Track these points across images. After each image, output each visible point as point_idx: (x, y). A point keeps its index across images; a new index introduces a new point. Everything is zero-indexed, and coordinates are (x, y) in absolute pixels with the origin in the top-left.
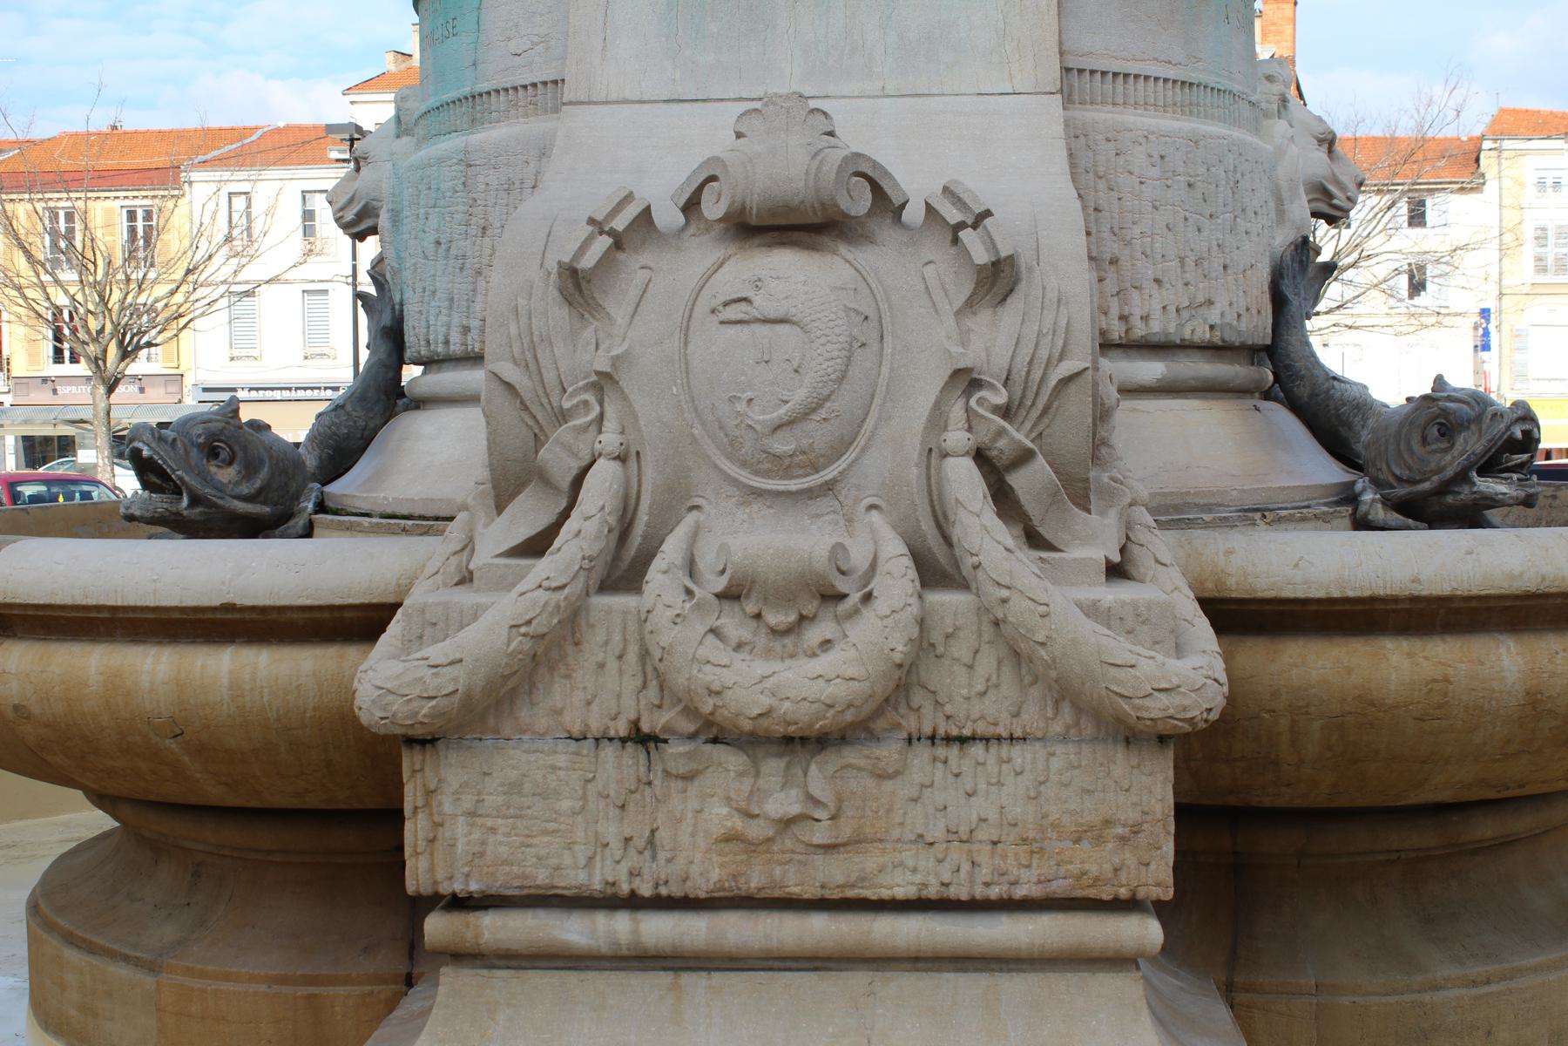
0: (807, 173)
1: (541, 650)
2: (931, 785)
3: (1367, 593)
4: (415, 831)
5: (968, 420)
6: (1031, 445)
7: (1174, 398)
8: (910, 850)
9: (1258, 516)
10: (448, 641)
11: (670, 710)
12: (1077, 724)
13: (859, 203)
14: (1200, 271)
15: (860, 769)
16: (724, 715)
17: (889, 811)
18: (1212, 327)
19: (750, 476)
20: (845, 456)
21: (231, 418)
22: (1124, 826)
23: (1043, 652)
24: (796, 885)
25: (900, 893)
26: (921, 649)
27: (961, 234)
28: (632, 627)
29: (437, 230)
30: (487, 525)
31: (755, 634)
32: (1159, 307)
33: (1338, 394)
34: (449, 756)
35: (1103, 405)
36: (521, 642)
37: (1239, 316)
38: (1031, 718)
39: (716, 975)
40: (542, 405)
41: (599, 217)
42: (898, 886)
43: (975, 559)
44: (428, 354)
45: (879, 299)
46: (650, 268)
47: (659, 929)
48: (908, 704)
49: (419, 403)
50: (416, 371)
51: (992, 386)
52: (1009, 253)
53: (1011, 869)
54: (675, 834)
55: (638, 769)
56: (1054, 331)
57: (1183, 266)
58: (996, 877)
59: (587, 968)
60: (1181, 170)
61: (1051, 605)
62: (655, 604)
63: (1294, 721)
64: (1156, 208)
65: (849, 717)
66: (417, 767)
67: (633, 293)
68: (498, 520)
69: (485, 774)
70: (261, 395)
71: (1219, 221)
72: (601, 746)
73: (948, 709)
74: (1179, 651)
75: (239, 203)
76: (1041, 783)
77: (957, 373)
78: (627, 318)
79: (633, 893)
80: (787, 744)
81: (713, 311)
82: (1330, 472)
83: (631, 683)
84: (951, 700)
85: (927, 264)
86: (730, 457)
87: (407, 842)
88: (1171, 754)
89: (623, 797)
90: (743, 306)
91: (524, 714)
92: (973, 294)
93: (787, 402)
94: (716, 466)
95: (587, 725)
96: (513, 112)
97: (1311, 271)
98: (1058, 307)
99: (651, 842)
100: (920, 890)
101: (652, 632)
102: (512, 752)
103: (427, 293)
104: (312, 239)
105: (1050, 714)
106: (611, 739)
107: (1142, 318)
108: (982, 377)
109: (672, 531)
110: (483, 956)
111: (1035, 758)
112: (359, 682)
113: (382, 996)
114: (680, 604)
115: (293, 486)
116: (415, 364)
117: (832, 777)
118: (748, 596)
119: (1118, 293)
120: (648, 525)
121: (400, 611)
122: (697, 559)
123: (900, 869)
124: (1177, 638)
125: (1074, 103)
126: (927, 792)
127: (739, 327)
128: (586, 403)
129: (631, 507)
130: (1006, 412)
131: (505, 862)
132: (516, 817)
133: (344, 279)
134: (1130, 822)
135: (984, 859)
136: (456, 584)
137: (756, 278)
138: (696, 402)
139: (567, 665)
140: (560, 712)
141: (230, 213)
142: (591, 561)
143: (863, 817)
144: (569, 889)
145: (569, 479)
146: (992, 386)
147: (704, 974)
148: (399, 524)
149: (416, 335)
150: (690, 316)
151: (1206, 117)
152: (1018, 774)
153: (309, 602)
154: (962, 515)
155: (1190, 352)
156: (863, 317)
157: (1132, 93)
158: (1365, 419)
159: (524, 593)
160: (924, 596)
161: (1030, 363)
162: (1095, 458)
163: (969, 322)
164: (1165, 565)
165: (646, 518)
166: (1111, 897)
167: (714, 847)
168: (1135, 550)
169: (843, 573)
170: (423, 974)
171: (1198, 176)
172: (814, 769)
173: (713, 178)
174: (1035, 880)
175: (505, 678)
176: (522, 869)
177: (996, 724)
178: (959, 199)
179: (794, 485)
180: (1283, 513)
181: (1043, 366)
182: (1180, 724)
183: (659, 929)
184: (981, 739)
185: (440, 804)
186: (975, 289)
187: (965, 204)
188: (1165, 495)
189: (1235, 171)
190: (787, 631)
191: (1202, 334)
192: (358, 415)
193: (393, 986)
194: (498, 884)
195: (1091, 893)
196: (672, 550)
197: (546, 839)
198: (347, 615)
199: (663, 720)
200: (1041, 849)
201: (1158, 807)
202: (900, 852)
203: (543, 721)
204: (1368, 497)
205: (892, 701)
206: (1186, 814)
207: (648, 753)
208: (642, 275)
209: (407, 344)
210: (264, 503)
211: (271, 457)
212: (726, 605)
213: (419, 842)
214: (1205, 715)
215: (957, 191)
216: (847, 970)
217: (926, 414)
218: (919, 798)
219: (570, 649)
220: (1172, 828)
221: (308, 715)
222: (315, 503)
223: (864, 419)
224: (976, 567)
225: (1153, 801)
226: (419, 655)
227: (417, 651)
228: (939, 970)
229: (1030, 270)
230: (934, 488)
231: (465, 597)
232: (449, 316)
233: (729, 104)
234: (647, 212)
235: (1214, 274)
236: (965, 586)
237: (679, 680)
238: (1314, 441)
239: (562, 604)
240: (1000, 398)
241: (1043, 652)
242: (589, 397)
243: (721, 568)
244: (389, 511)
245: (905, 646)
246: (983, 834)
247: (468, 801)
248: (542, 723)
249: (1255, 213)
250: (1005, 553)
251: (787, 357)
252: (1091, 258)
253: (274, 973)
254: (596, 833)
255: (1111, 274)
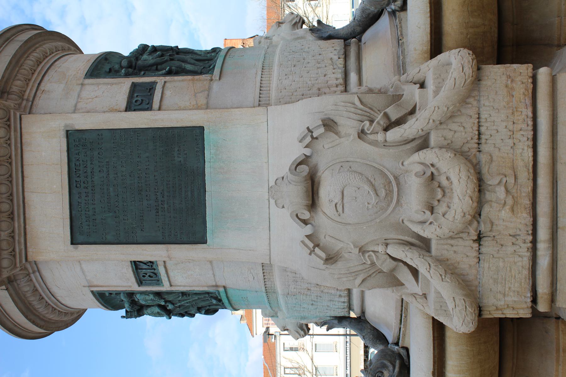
0: (296, 185)
1: (450, 271)
2: (494, 144)
3: (428, 5)
4: (510, 314)
5: (374, 133)
6: (382, 113)
7: (362, 69)
8: (516, 151)
9: (400, 42)
10: (447, 302)
11: (469, 230)
12: (474, 97)
13: (305, 169)
14: (322, 62)
15: (489, 168)
16: (472, 213)
17: (503, 157)
18: (339, 58)
19: (393, 203)
20: (386, 173)
21: (368, 372)
22: (508, 81)
23: (451, 108)
24: (528, 188)
25: (531, 154)
26: (449, 148)
27: (315, 136)
28: (442, 242)
29: (308, 304)
30: (407, 289)
31: (444, 202)
32: (333, 75)
33: (359, 18)
34: (485, 302)
35: (368, 91)
36: (447, 278)
37: (335, 50)
38: (472, 112)
39: (559, 215)
40: (369, 270)
41: (309, 251)
42: (528, 155)
43: (420, 131)
44: (347, 308)
45: (335, 162)
46: (325, 235)
47: (543, 234)
48: (467, 152)
49: (363, 312)
50: (352, 313)
51: (363, 126)
52: (321, 121)
53: (522, 118)
54: (511, 228)
55: (489, 240)
56: (345, 106)
57: (320, 68)
58: (525, 122)
59: (557, 258)
60: (290, 69)
61: (435, 106)
62: (435, 234)
63: (470, 27)
64: (302, 77)
65: (472, 171)
66: (488, 313)
67: (333, 241)
68: (406, 285)
69: (491, 291)
70: (348, 366)
71: (305, 57)
72: (482, 252)
73: (469, 139)
74: (449, 64)
75: (288, 371)
76: (494, 108)
77: (359, 137)
78: (341, 243)
79: (531, 242)
80: (481, 191)
81: (340, 215)
82: (385, 20)
83: (461, 242)
84: (466, 138)
85: (324, 147)
86: (386, 210)
87: (511, 317)
88: (484, 66)
89: (499, 245)
90: (338, 206)
91: (471, 277)
92: (333, 132)
93: (369, 191)
94: (389, 214)
95: (475, 257)
96: (272, 280)
97: (320, 28)
98: (338, 105)
99: (514, 236)
100: (530, 148)
101: (444, 235)
102: (484, 281)
103: (328, 308)
104: (299, 348)
105: (470, 106)
106: (479, 249)
107: (337, 80)
108: (360, 129)
109: (410, 229)
110: (552, 292)
111: (485, 110)
112: (460, 331)
113: (563, 327)
114: (435, 226)
115: (390, 353)
116: (350, 313)
117: (492, 176)
118: (432, 204)
119: (329, 88)
120: (408, 236)
121: (436, 318)
122: (420, 221)
123: (523, 154)
124: (444, 65)
125: (269, 103)
126: (497, 145)
127: (345, 207)
128: (369, 256)
129: (404, 242)
130: (372, 121)
131: (521, 284)
132: (505, 280)
133: (312, 339)
134: (507, 79)
135: (519, 127)
136: (426, 299)
137: (329, 202)
138: (369, 221)
139: (454, 263)
140: (470, 266)
141: (290, 374)
142: (421, 255)
143: (505, 166)
144: (530, 263)
145: (393, 262)
146: (363, 126)
147: (558, 219)
148: (404, 319)
149: (341, 312)
150: (341, 223)
151: (273, 62)
152: (491, 116)
153: (432, 347)
154: (405, 135)
155: (347, 65)
156: (341, 168)
157: (266, 85)
158: (367, 9)
159: (431, 277)
160: (432, 147)
161: (356, 114)
162: (385, 93)
163: (343, 134)
164: (420, 70)
165: (406, 237)
166: (532, 85)
167: (515, 215)
168: (415, 79)
169: (425, 173)
170: (556, 314)
171: (291, 64)
172: (489, 183)
173: (297, 216)
174: (526, 110)
175: (459, 283)
176: (523, 279)
177: (474, 123)
178: (303, 137)
179: (395, 189)
180: (399, 33)
181: (357, 110)
182: (474, 63)
183: (543, 234)
184: (479, 128)
185: (501, 305)
186: (332, 132)
187: (305, 135)
188: (394, 72)
189: (289, 52)
190: (444, 191)
191: (341, 61)
192: (366, 331)
193: (560, 323)
194: (528, 287)
195: (530, 91)
196: (417, 229)
197: (513, 271)
198: (436, 335)
199: (473, 232)
200: (516, 108)
201: (501, 70)
202: (517, 154)
203: (473, 271)
204: (393, 7)
205: (466, 157)
206: (500, 61)
207: (484, 237)
208: (327, 238)
209: (344, 315)
210: (395, 362)
211: (380, 360)
212: (435, 211)
213: (514, 312)
214: (471, 55)
215: (301, 138)
216: (557, 172)
217: (373, 147)
218: (499, 148)
219: (449, 262)
220: (509, 65)
221: (469, 349)
222: (396, 346)
223: (374, 167)
224: (423, 130)
225: (499, 71)
226: (451, 312)
227: (450, 312)
228: (557, 141)
229: (326, 115)
230: (396, 144)
231: (432, 296)
232: (335, 301)
233: (270, 211)
234: (307, 236)
235: (322, 58)
236: (428, 134)
237: (460, 226)
238: (374, 25)
239: (435, 264)
240: (367, 123)
241: (451, 108)
242: (367, 255)
243: (423, 213)
244: (399, 322)
245: (448, 153)
246: (511, 127)
247: (500, 296)
248: (474, 271)
249: (302, 45)
250: (418, 121)
251: (354, 192)
252: (318, 96)
253: (555, 362)
254: (510, 254)
255: (323, 90)
